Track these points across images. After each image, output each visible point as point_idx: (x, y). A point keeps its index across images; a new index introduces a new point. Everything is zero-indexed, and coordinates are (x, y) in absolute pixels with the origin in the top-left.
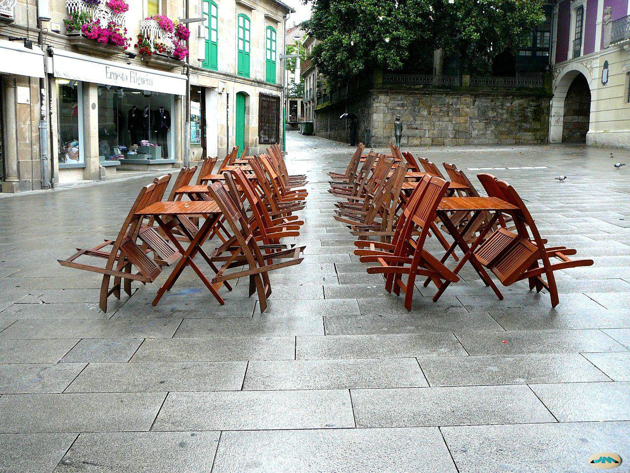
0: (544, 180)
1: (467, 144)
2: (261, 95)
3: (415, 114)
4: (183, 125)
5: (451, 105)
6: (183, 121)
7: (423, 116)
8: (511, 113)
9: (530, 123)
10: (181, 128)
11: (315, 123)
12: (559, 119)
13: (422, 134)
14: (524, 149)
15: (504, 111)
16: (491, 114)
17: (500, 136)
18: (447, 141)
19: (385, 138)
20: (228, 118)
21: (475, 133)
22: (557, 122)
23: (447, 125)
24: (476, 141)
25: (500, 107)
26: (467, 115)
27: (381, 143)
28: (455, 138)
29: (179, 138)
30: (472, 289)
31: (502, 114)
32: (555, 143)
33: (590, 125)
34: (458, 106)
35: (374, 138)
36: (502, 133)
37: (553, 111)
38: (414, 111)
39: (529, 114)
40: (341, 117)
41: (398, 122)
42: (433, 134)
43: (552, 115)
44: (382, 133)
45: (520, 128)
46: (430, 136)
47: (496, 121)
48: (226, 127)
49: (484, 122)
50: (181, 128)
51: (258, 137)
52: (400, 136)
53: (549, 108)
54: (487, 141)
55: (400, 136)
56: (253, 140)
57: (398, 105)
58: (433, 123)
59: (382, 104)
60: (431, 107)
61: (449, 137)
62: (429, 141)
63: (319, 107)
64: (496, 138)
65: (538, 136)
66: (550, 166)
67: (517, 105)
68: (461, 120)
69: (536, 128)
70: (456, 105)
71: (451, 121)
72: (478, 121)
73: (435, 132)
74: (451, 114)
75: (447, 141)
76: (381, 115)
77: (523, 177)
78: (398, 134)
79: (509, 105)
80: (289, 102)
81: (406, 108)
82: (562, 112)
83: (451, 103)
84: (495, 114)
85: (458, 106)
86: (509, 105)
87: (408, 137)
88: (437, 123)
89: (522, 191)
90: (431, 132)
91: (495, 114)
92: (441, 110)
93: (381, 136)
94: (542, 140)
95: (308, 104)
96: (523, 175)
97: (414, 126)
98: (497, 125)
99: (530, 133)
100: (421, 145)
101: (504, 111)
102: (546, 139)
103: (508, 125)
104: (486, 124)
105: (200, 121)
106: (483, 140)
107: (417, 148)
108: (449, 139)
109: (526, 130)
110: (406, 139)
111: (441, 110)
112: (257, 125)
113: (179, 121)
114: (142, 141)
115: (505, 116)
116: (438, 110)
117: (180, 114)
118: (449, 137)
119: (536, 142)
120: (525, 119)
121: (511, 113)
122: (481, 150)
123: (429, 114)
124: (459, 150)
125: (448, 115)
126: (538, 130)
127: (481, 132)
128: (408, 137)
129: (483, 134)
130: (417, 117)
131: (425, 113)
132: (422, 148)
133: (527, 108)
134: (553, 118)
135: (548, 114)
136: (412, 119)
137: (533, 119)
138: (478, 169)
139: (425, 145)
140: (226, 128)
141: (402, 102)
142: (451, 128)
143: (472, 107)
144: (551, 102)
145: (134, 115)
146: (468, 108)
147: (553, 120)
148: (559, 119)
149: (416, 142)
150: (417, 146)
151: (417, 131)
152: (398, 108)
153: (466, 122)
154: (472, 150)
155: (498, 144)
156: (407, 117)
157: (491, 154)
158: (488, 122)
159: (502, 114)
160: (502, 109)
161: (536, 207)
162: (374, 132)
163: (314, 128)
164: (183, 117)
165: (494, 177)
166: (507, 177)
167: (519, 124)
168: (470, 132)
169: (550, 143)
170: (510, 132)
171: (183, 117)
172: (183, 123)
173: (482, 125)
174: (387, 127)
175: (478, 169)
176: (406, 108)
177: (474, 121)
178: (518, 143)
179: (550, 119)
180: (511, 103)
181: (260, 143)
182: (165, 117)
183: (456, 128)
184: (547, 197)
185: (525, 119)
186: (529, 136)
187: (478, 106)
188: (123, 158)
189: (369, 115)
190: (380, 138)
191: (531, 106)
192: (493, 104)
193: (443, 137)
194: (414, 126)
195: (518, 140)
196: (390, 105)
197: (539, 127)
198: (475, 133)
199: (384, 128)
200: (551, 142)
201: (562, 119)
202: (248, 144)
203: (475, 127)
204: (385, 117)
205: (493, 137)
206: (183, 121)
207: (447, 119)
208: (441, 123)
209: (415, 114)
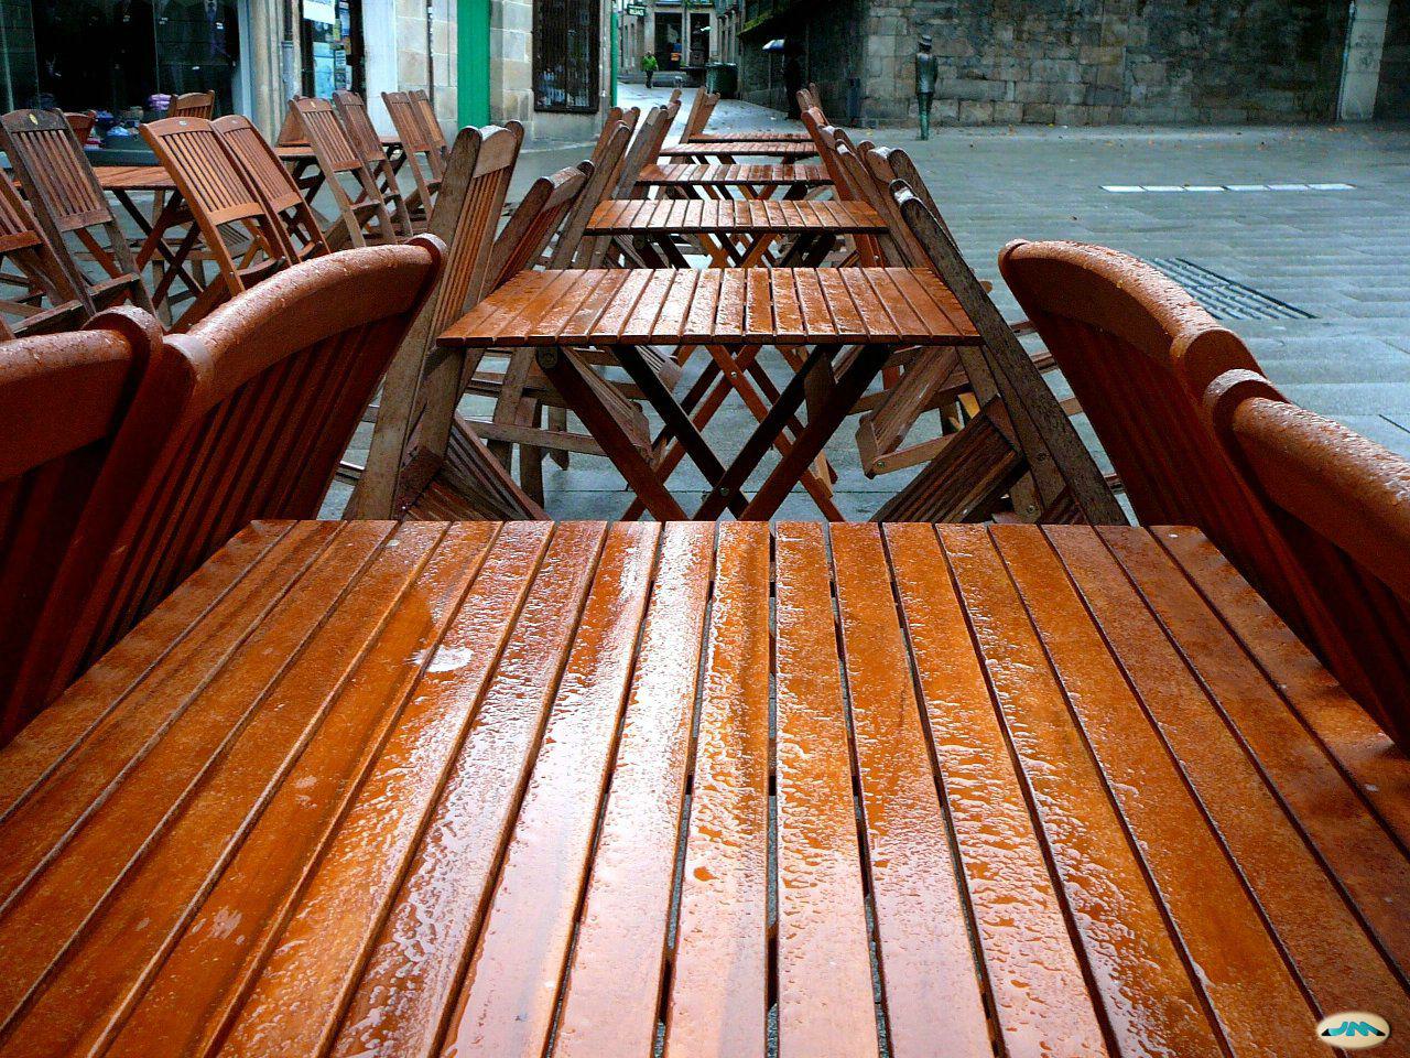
0: (1350, 227)
1: (1116, 121)
2: (657, 15)
3: (979, 38)
4: (274, 49)
5: (1079, 13)
6: (274, 38)
7: (1002, 45)
8: (1240, 36)
9: (1291, 66)
10: (270, 57)
11: (740, 70)
12: (1371, 54)
13: (996, 94)
14: (1271, 134)
15: (1222, 32)
16: (1184, 39)
17: (1204, 100)
18: (1062, 112)
19: (899, 101)
20: (429, 35)
21: (1138, 91)
22: (1365, 62)
23: (1066, 69)
24: (1141, 114)
25: (1211, 20)
26: (1119, 41)
27: (883, 115)
28: (1084, 104)
29: (265, 89)
30: (1053, 768)
31: (1214, 41)
32: (1356, 121)
33: (692, 385)
34: (1097, 18)
35: (868, 102)
36: (1210, 92)
37: (1357, 32)
38: (979, 29)
39: (1288, 41)
40: (767, 46)
41: (925, 56)
42: (1029, 93)
43: (1353, 44)
44: (891, 88)
45: (1263, 81)
46: (1020, 98)
47: (1196, 58)
48: (425, 61)
49: (1164, 60)
50: (270, 57)
51: (530, 93)
52: (930, 96)
53: (1344, 24)
54: (1170, 114)
55: (930, 96)
56: (516, 100)
57: (937, 14)
58: (1026, 63)
59: (893, 10)
60: (1022, 18)
61: (1068, 102)
62: (1013, 112)
63: (751, 24)
64: (1194, 105)
65: (1309, 103)
66: (1362, 183)
67: (1259, 15)
68: (1105, 55)
69: (1305, 78)
70: (1092, 14)
71: (1074, 58)
72: (1148, 58)
73: (1033, 87)
74: (1076, 40)
75: (1062, 112)
76: (890, 41)
77: (1278, 218)
78: (925, 88)
79: (1235, 14)
80: (689, 17)
81: (956, 21)
82: (1380, 34)
83: (1077, 9)
84: (1197, 38)
85: (1097, 18)
86: (1235, 14)
87: (961, 100)
88: (1038, 64)
89: (1284, 268)
90: (1022, 86)
91: (1197, 38)
92: (1050, 28)
93: (887, 97)
94: (1320, 110)
95: (727, 21)
96: (1280, 210)
97: (976, 71)
98: (1200, 69)
99: (1290, 94)
100: (993, 123)
101: (1222, 32)
102: (1332, 108)
103: (1229, 70)
104: (1171, 67)
105: (347, 42)
106: (1158, 111)
107: (980, 130)
108: (1068, 107)
109: (1279, 85)
110: (955, 107)
111: (1050, 28)
112: (527, 59)
113: (263, 37)
114: (154, 97)
115: (1222, 46)
116: (1042, 27)
117: (263, 17)
118: (1068, 102)
119: (1302, 117)
120: (1276, 54)
121: (1239, 36)
122: (1152, 137)
123: (1018, 38)
124: (1093, 135)
125: (1069, 41)
126: (1309, 85)
127: (1157, 89)
128: (961, 100)
129: (1159, 94)
130: (986, 47)
131: (1007, 35)
132: (993, 131)
133: (1285, 24)
134: (1353, 52)
135: (1342, 39)
136: (971, 51)
137: (1300, 56)
138: (1138, 189)
139: (1004, 123)
140: (426, 65)
141: (948, 5)
142: (1073, 76)
143: (1134, 19)
144: (1352, 5)
145: (127, 18)
146: (1124, 21)
147: (1352, 58)
148: (1371, 54)
149: (980, 113)
150: (984, 124)
151: (984, 85)
152: (936, 22)
153: (1116, 60)
154: (1126, 137)
155: (1198, 123)
156: (959, 47)
157: (1179, 145)
158: (1175, 61)
159: (1214, 41)
160: (1216, 25)
161: (1346, 349)
162: (869, 85)
163: (739, 80)
164: (273, 26)
165: (1193, 320)
166: (1228, 217)
167: (1259, 68)
168: (1127, 89)
169: (1342, 121)
170: (1232, 90)
171: (273, 26)
172: (274, 45)
173: (1159, 69)
174: (904, 73)
175: (1138, 189)
176: (956, 21)
177: (1138, 59)
178: (1254, 119)
179: (1345, 55)
180: (1243, 10)
181: (538, 109)
182: (220, 26)
183: (1089, 78)
184: (1382, 298)
185: (1276, 54)
186: (1284, 101)
187: (1150, 18)
188: (96, 147)
189: (860, 40)
190: (886, 102)
191: (1296, 17)
192: (1192, 11)
193: (1052, 100)
194: (976, 71)
195: (1253, 114)
196: (914, 13)
197: (1314, 77)
198: (1138, 91)
199: (898, 76)
200: (1344, 117)
201: (1378, 54)
202: (499, 109)
203: (1139, 74)
204: (899, 45)
205: (1187, 104)
206: (274, 38)
207: (1064, 52)
208: (1048, 62)
209: (979, 38)
